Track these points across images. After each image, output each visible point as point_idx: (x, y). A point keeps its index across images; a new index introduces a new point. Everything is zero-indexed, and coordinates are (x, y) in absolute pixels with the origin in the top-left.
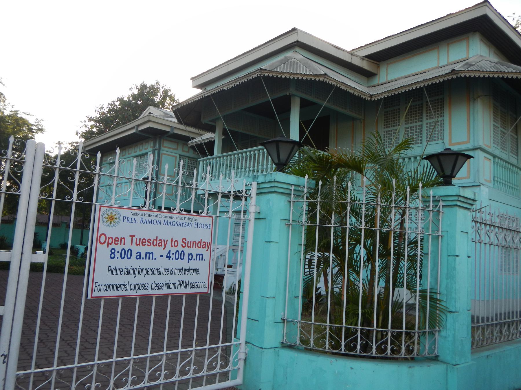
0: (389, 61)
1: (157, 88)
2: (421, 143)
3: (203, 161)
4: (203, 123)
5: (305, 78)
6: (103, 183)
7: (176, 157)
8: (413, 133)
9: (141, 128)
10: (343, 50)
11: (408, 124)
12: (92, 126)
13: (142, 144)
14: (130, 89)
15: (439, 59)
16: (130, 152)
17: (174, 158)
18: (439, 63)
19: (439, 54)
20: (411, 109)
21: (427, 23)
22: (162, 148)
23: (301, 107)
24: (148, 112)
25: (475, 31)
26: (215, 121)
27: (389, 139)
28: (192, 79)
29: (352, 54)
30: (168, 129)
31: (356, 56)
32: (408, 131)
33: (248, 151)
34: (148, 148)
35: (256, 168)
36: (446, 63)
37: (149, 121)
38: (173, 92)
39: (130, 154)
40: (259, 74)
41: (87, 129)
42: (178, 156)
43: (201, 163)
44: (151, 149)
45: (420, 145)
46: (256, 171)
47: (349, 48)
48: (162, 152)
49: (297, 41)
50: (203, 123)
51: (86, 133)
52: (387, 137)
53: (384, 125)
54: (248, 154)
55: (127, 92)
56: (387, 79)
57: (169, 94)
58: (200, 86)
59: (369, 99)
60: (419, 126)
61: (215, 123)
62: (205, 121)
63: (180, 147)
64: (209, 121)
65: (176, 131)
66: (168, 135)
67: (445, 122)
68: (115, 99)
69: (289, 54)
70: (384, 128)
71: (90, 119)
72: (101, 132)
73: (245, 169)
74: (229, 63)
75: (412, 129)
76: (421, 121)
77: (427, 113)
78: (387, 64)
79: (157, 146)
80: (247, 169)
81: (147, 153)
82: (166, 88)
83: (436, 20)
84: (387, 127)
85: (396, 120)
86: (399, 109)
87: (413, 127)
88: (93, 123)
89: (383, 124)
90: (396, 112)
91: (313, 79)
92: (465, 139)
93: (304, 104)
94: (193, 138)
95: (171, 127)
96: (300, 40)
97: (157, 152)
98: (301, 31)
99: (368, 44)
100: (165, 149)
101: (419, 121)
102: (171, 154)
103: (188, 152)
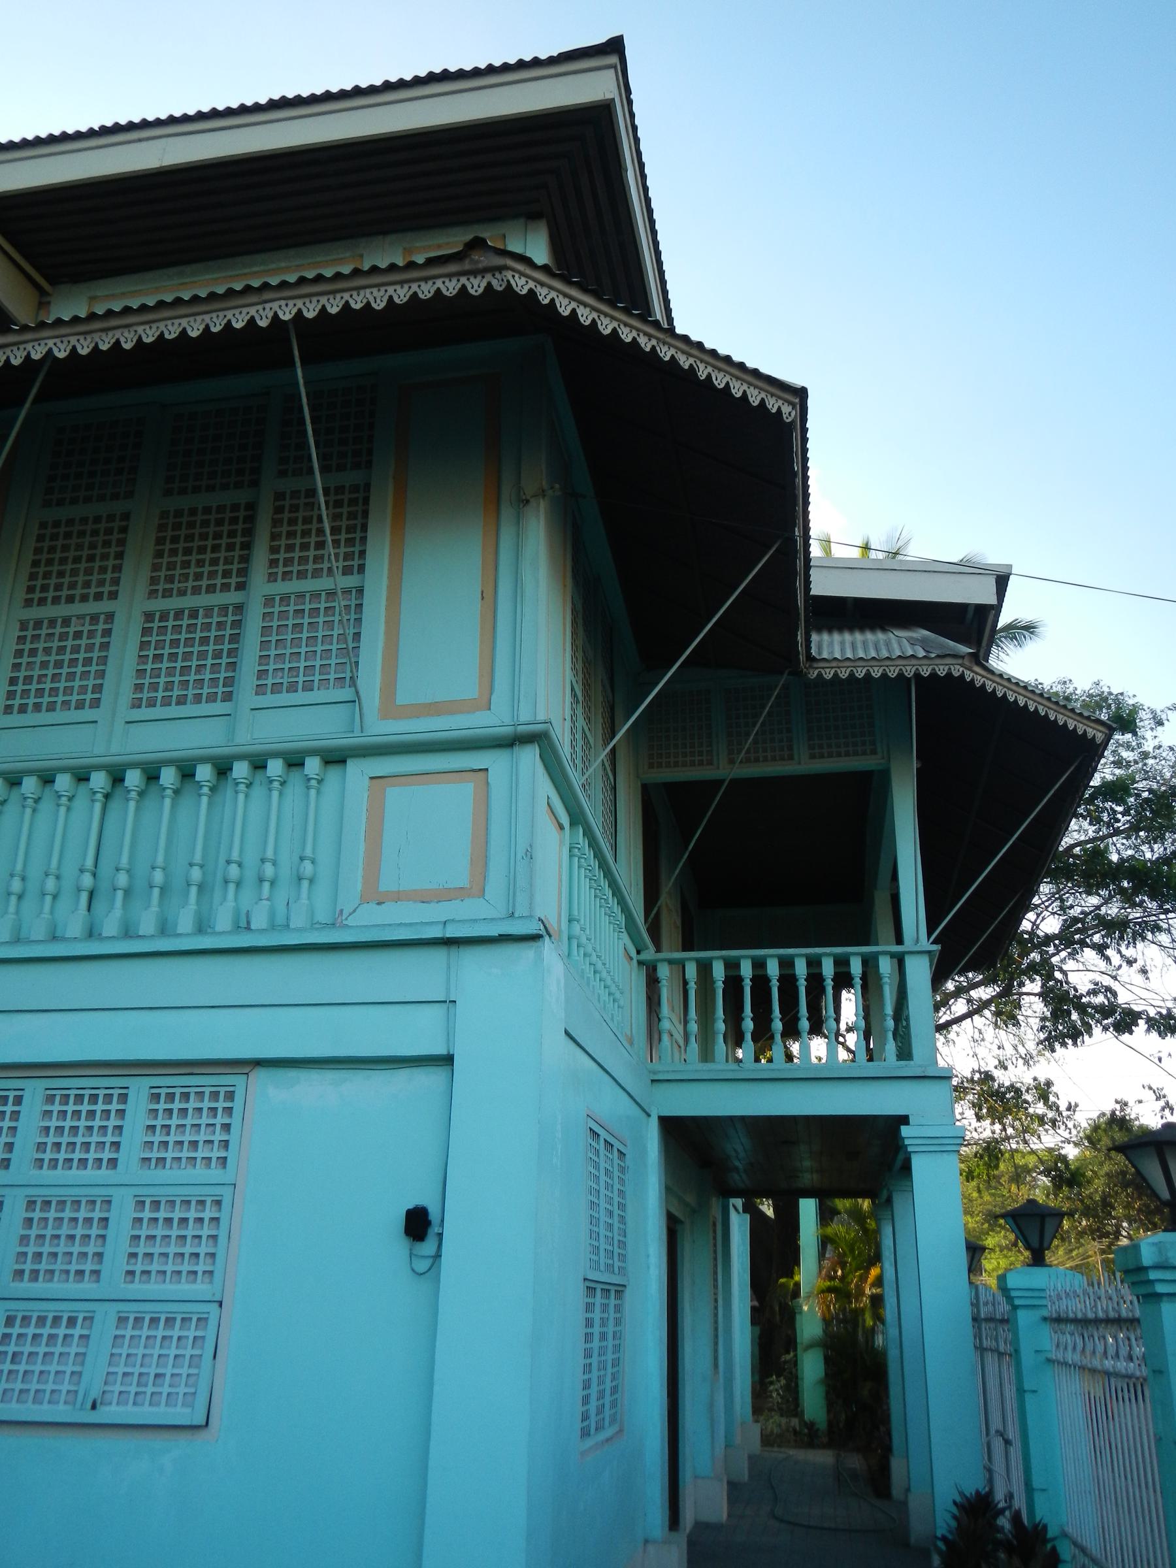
11: (167, 594)
25: (532, 216)
27: (44, 665)
32: (162, 630)
52: (33, 652)
60: (224, 609)
76: (241, 587)
77: (274, 550)
87: (194, 614)
92: (470, 690)
101: (226, 587)
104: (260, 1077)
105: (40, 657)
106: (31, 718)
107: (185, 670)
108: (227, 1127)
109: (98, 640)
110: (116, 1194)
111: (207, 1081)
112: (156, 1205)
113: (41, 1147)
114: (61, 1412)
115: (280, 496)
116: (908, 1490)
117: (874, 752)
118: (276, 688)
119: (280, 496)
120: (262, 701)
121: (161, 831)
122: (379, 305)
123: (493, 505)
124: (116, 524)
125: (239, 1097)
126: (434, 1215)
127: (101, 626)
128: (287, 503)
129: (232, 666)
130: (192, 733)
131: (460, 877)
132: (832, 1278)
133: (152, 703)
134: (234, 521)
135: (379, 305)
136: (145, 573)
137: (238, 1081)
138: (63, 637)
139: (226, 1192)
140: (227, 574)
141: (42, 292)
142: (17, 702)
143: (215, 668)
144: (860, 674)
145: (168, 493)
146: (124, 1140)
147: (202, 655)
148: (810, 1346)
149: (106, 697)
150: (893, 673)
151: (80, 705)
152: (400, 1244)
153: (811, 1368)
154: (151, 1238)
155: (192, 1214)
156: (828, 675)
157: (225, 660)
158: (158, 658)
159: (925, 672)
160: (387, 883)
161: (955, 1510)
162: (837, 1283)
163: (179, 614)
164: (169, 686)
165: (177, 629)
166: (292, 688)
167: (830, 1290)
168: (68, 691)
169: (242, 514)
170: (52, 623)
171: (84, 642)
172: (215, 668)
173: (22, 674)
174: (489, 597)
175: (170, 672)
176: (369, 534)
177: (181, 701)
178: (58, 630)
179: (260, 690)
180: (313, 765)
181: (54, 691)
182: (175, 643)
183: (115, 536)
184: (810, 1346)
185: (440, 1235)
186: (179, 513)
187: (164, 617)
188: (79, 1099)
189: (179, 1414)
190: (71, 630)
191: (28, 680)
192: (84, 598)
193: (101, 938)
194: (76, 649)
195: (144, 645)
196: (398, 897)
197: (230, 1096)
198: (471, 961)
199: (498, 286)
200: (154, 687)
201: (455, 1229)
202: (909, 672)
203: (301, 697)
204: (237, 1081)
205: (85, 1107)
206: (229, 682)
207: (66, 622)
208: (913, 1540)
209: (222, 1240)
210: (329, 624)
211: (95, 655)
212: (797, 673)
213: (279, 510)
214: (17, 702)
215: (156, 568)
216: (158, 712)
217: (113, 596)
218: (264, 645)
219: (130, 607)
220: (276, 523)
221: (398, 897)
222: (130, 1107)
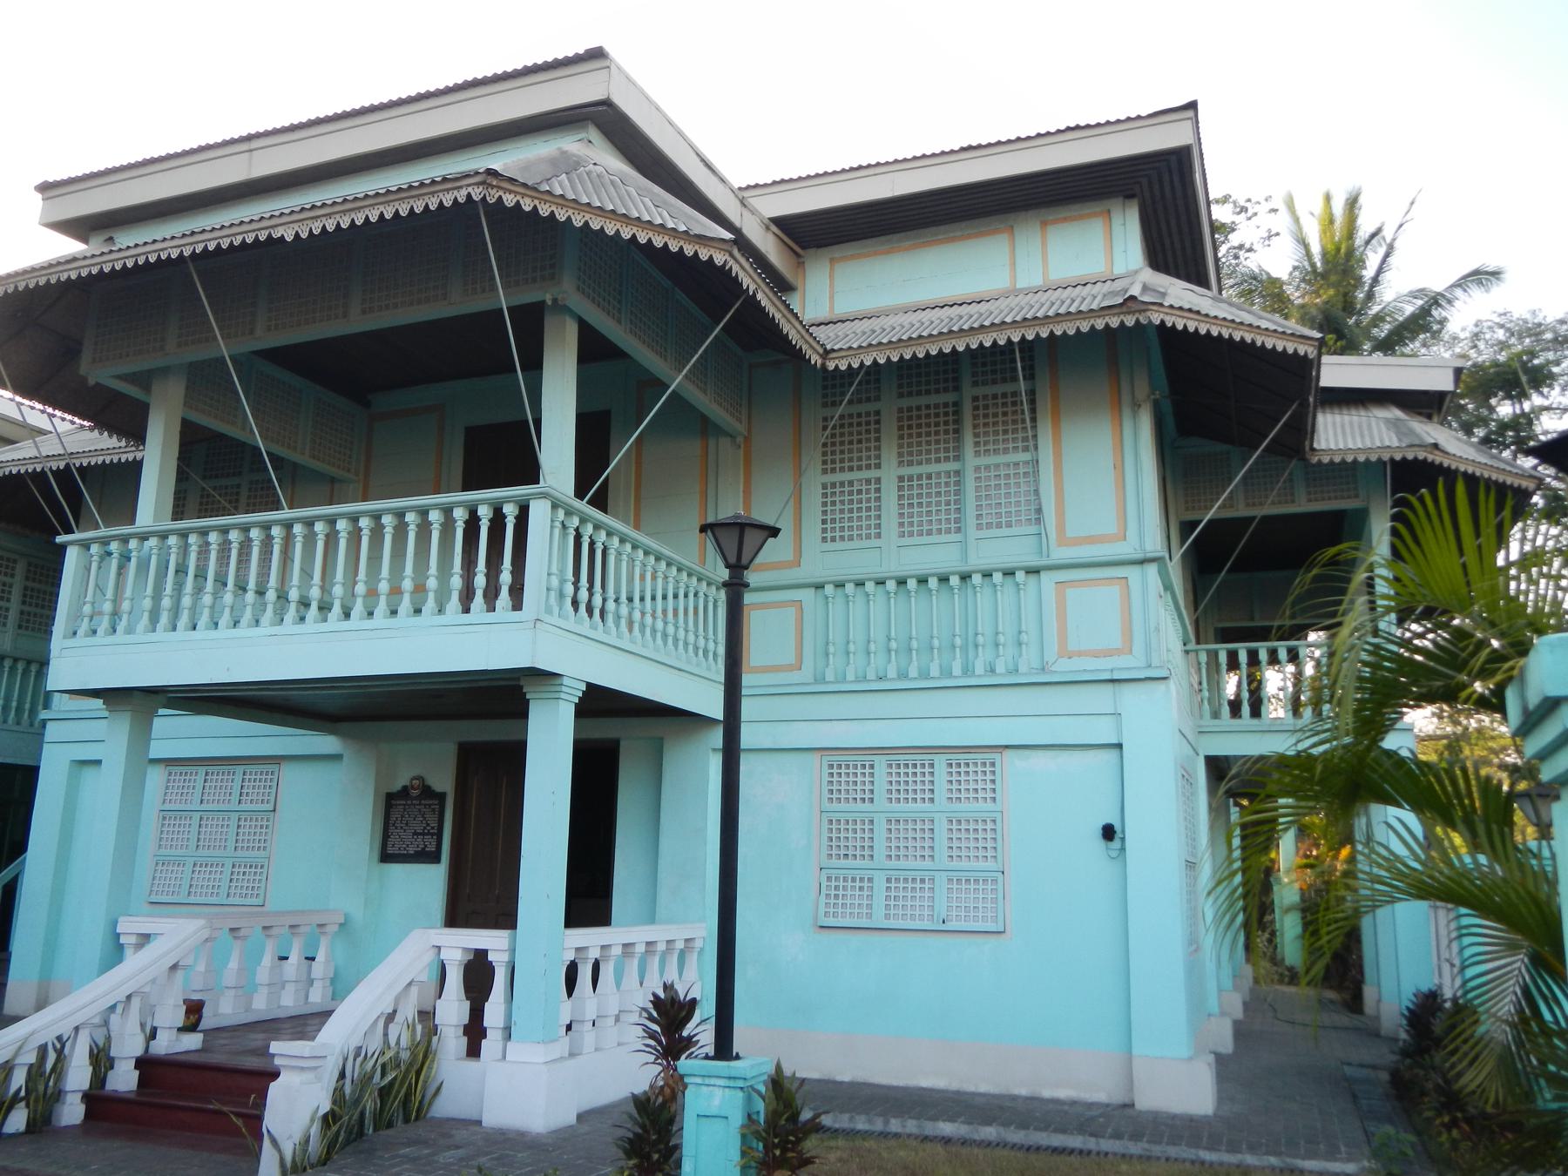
0: (837, 251)
3: (85, 545)
8: (929, 495)
11: (910, 463)
15: (1013, 264)
18: (1014, 277)
19: (1044, 244)
21: (999, 143)
23: (583, 359)
25: (1129, 197)
26: (144, 380)
27: (842, 511)
28: (45, 188)
29: (743, 203)
31: (753, 212)
32: (911, 487)
33: (213, 528)
35: (315, 593)
36: (1037, 281)
45: (953, 537)
49: (607, 103)
50: (91, 382)
52: (834, 503)
56: (832, 308)
60: (948, 474)
61: (147, 389)
62: (100, 372)
64: (119, 377)
69: (569, 144)
73: (261, 593)
74: (255, 144)
76: (957, 458)
77: (976, 435)
80: (271, 595)
84: (833, 470)
85: (869, 449)
86: (878, 413)
87: (929, 477)
89: (820, 459)
91: (689, 251)
92: (1112, 528)
93: (594, 350)
96: (618, 100)
101: (947, 459)
104: (1008, 753)
105: (838, 507)
108: (993, 781)
109: (873, 495)
110: (936, 816)
112: (959, 822)
113: (890, 791)
114: (926, 925)
115: (975, 399)
116: (1379, 1001)
117: (1357, 496)
119: (975, 399)
120: (982, 534)
121: (935, 614)
122: (1071, 332)
123: (1117, 405)
124: (872, 418)
125: (998, 765)
126: (1117, 828)
127: (873, 487)
128: (981, 403)
129: (958, 510)
130: (938, 555)
131: (1116, 641)
132: (1307, 857)
133: (911, 534)
134: (946, 414)
135: (1071, 332)
136: (895, 450)
137: (997, 757)
139: (998, 816)
140: (947, 450)
142: (829, 535)
144: (1350, 459)
145: (901, 395)
147: (938, 503)
148: (1288, 910)
150: (1374, 458)
152: (1101, 843)
153: (1289, 927)
155: (971, 827)
156: (1326, 460)
157: (953, 507)
159: (1398, 457)
160: (1072, 646)
162: (1311, 861)
163: (920, 477)
164: (920, 524)
166: (999, 526)
167: (1307, 866)
168: (860, 528)
169: (951, 410)
170: (842, 484)
171: (864, 496)
172: (948, 512)
174: (1119, 467)
175: (920, 514)
176: (1039, 424)
177: (929, 533)
178: (846, 489)
180: (1020, 576)
181: (851, 528)
182: (920, 496)
183: (873, 427)
184: (1288, 910)
185: (1123, 839)
186: (910, 409)
188: (907, 766)
189: (991, 927)
191: (833, 521)
192: (860, 468)
195: (900, 497)
196: (1080, 654)
197: (993, 764)
198: (1129, 694)
199: (1143, 321)
201: (1133, 833)
202: (1386, 457)
203: (1005, 531)
205: (910, 770)
206: (957, 521)
207: (851, 483)
208: (1383, 1033)
210: (1018, 485)
211: (873, 504)
212: (1303, 459)
213: (976, 408)
214: (829, 535)
216: (916, 540)
218: (978, 498)
219: (890, 472)
220: (975, 417)
221: (1080, 654)
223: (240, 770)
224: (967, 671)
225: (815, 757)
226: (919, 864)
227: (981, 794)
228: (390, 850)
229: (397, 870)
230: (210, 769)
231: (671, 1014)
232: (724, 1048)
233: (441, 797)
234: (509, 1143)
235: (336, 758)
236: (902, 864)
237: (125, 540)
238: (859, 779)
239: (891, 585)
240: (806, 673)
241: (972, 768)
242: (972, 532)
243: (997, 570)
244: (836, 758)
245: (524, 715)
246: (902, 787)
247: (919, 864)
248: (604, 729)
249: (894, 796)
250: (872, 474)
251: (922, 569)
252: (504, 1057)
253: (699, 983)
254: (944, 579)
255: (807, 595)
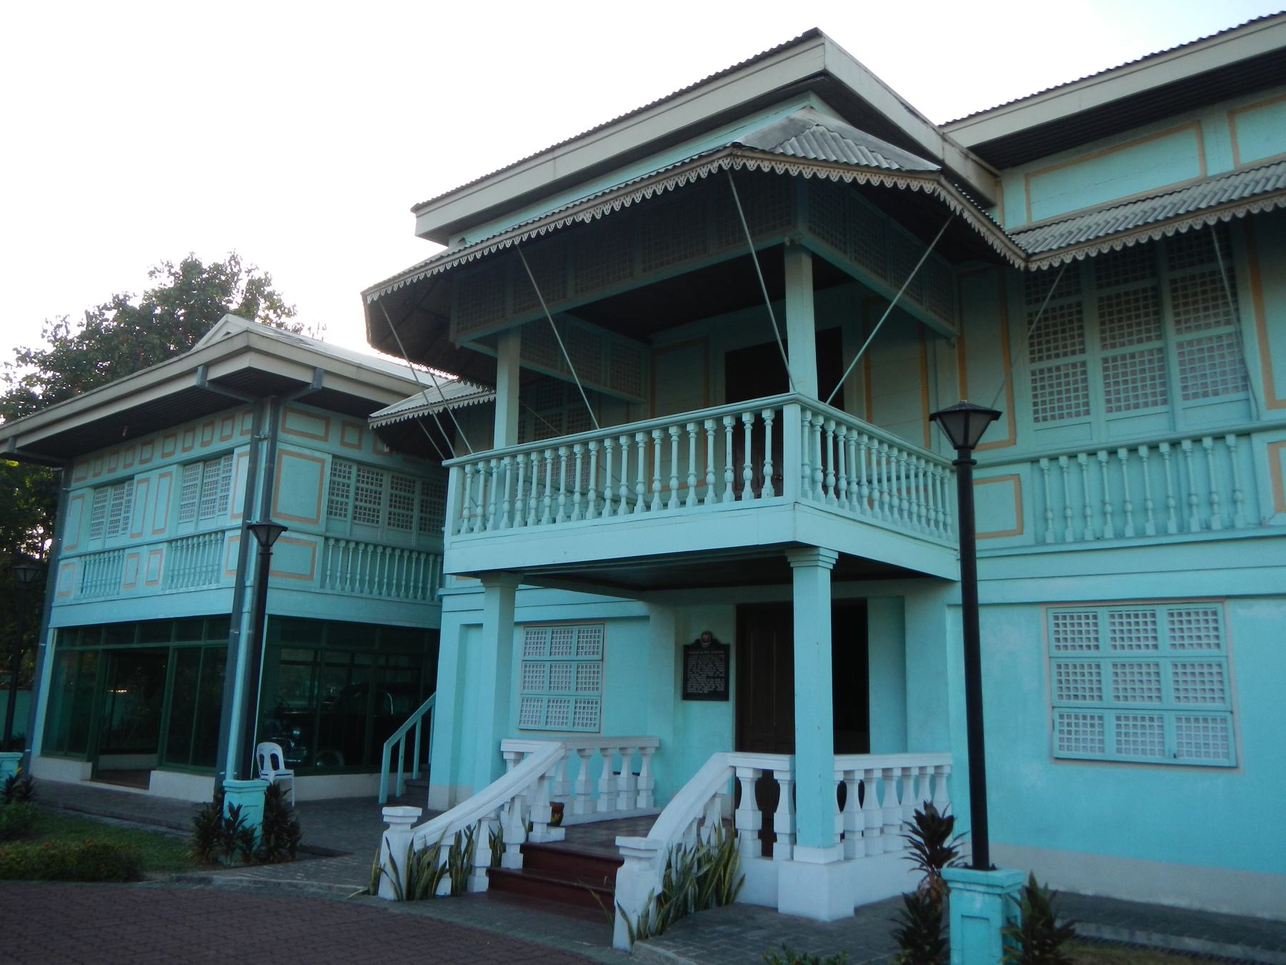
1: (234, 274)
2: (1165, 402)
4: (458, 346)
5: (875, 181)
6: (71, 548)
7: (322, 461)
8: (1134, 373)
9: (216, 373)
10: (925, 121)
11: (1113, 346)
12: (30, 379)
13: (212, 423)
14: (152, 274)
16: (146, 455)
17: (318, 465)
19: (1027, 191)
20: (1046, 319)
22: (281, 435)
23: (818, 286)
24: (224, 331)
26: (492, 341)
27: (1051, 394)
28: (417, 209)
29: (944, 138)
30: (305, 376)
31: (953, 144)
32: (1115, 367)
34: (235, 435)
35: (623, 491)
36: (1229, 166)
37: (247, 349)
38: (275, 287)
39: (171, 454)
40: (726, 163)
41: (15, 386)
42: (329, 458)
43: (453, 473)
44: (247, 438)
46: (623, 501)
47: (938, 118)
48: (280, 446)
49: (824, 73)
50: (458, 346)
51: (8, 401)
52: (1043, 387)
53: (1032, 352)
54: (548, 454)
55: (139, 280)
56: (1029, 217)
57: (268, 289)
58: (439, 235)
59: (1023, 265)
61: (495, 347)
62: (464, 340)
63: (335, 434)
64: (475, 341)
65: (330, 384)
66: (302, 394)
67: (1246, 338)
68: (109, 300)
70: (1033, 360)
71: (25, 358)
72: (57, 396)
74: (557, 153)
75: (1054, 374)
76: (1159, 337)
78: (1027, 176)
79: (266, 429)
80: (592, 495)
81: (230, 452)
82: (257, 275)
83: (963, 120)
84: (1041, 359)
88: (32, 369)
90: (1071, 314)
91: (902, 184)
93: (827, 280)
94: (384, 406)
95: (314, 368)
97: (264, 447)
98: (833, 43)
99: (978, 114)
100: (290, 437)
102: (307, 452)
103: (359, 447)
104: (1230, 604)
106: (1050, 423)
107: (1135, 389)
109: (1079, 377)
110: (1161, 661)
111: (1200, 607)
114: (1157, 758)
115: (1173, 282)
118: (1196, 396)
119: (1173, 282)
137: (1218, 607)
138: (1058, 377)
141: (995, 176)
142: (1040, 415)
143: (1153, 386)
146: (1159, 635)
147: (1143, 380)
149: (1092, 407)
151: (1078, 414)
154: (1185, 681)
158: (1117, 383)
161: (906, 909)
164: (1127, 399)
165: (1125, 366)
170: (1050, 370)
171: (1071, 379)
172: (1153, 386)
173: (1039, 400)
175: (1126, 390)
179: (1186, 397)
180: (1231, 440)
186: (1109, 298)
187: (1115, 359)
190: (1062, 373)
191: (1044, 403)
193: (1189, 532)
194: (1068, 384)
195: (1106, 377)
200: (1118, 400)
204: (1218, 607)
205: (1133, 620)
209: (1226, 681)
213: (1175, 290)
214: (1040, 415)
215: (1103, 332)
217: (1083, 351)
218: (1183, 371)
219: (1094, 356)
222: (1158, 619)
223: (576, 629)
224: (1120, 535)
225: (1040, 611)
226: (1147, 704)
227: (1204, 641)
228: (690, 690)
229: (696, 706)
230: (555, 629)
231: (931, 829)
232: (981, 860)
233: (726, 648)
234: (800, 926)
235: (645, 618)
236: (1130, 703)
237: (487, 460)
238: (1084, 628)
239: (1103, 456)
240: (1028, 536)
241: (1193, 618)
242: (1179, 403)
243: (1063, 454)
244: (1061, 611)
245: (789, 580)
246: (1126, 635)
247: (1147, 704)
248: (854, 590)
249: (1118, 643)
250: (1078, 358)
251: (1132, 439)
252: (792, 858)
253: (953, 801)
254: (1113, 452)
255: (1024, 470)
